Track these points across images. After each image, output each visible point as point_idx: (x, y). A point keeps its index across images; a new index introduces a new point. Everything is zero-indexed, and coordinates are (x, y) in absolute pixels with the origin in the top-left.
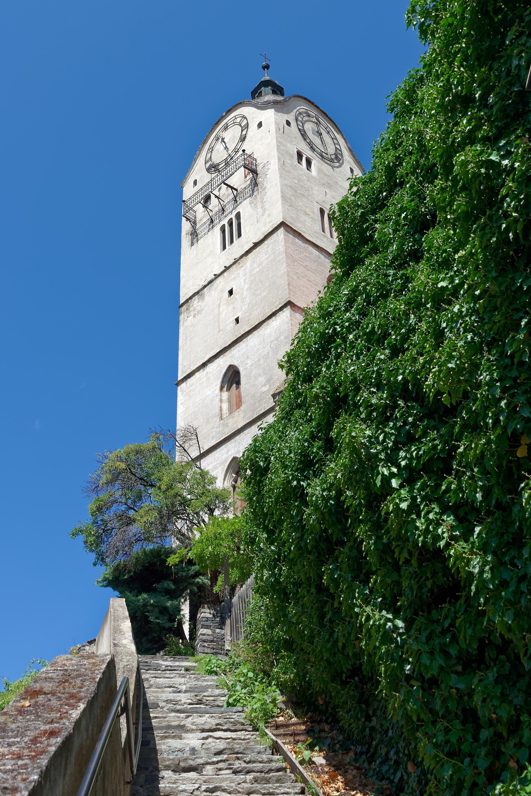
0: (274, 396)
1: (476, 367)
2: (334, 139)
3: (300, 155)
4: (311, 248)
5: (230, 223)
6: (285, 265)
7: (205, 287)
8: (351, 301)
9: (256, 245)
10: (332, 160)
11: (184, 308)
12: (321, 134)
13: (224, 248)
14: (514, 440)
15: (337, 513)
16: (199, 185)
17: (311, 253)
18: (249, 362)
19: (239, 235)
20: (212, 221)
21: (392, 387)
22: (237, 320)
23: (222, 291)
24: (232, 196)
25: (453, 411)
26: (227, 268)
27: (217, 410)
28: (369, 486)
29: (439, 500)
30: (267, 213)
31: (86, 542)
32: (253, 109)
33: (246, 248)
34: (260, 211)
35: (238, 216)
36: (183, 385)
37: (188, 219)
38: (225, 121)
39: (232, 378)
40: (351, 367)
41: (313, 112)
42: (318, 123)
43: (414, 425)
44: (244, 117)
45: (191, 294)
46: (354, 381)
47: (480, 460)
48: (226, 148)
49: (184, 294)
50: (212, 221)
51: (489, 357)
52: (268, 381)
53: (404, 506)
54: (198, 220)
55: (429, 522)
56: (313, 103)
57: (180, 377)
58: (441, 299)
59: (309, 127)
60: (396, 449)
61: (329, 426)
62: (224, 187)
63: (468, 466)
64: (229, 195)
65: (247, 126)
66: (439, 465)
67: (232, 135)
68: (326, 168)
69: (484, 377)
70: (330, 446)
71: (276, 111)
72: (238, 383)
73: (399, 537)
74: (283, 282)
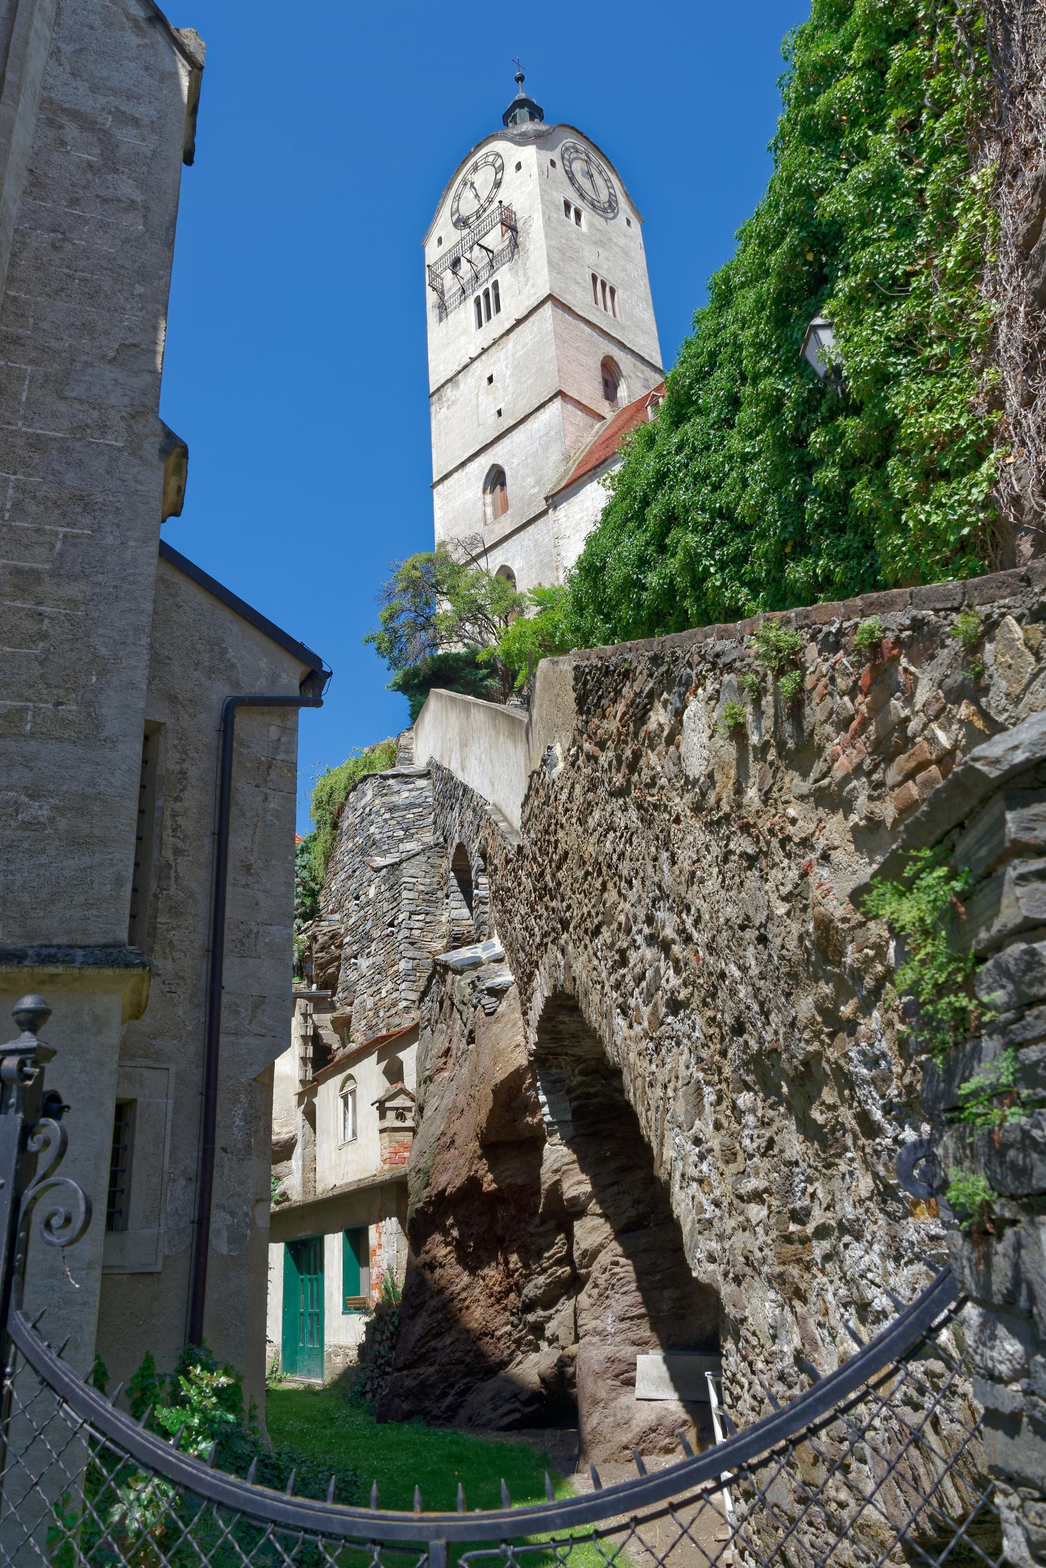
0: (547, 499)
1: (766, 502)
2: (607, 181)
3: (567, 206)
4: (582, 325)
5: (486, 294)
6: (554, 347)
7: (459, 372)
8: (680, 449)
9: (519, 322)
10: (604, 210)
11: (435, 398)
12: (592, 176)
13: (480, 325)
14: (784, 542)
15: (670, 593)
16: (446, 245)
17: (583, 331)
18: (515, 461)
19: (498, 309)
20: (464, 292)
21: (712, 511)
22: (499, 413)
23: (480, 378)
24: (487, 260)
25: (751, 527)
26: (484, 351)
27: (481, 515)
28: (694, 571)
29: (739, 579)
30: (531, 282)
31: (379, 648)
32: (509, 145)
33: (507, 326)
34: (522, 279)
35: (495, 285)
36: (440, 487)
37: (434, 289)
38: (473, 160)
39: (496, 478)
40: (681, 495)
41: (582, 146)
42: (588, 161)
43: (726, 534)
44: (498, 155)
45: (442, 381)
46: (684, 506)
47: (765, 555)
48: (477, 196)
49: (435, 380)
50: (464, 292)
51: (773, 498)
52: (538, 482)
53: (718, 583)
54: (446, 289)
55: (733, 592)
56: (581, 134)
57: (435, 479)
58: (747, 459)
59: (577, 166)
60: (713, 549)
61: (665, 534)
62: (476, 248)
63: (759, 559)
64: (483, 258)
65: (502, 167)
66: (741, 558)
67: (483, 179)
68: (598, 221)
69: (770, 509)
70: (662, 549)
71: (539, 148)
72: (503, 484)
73: (713, 604)
74: (552, 367)
